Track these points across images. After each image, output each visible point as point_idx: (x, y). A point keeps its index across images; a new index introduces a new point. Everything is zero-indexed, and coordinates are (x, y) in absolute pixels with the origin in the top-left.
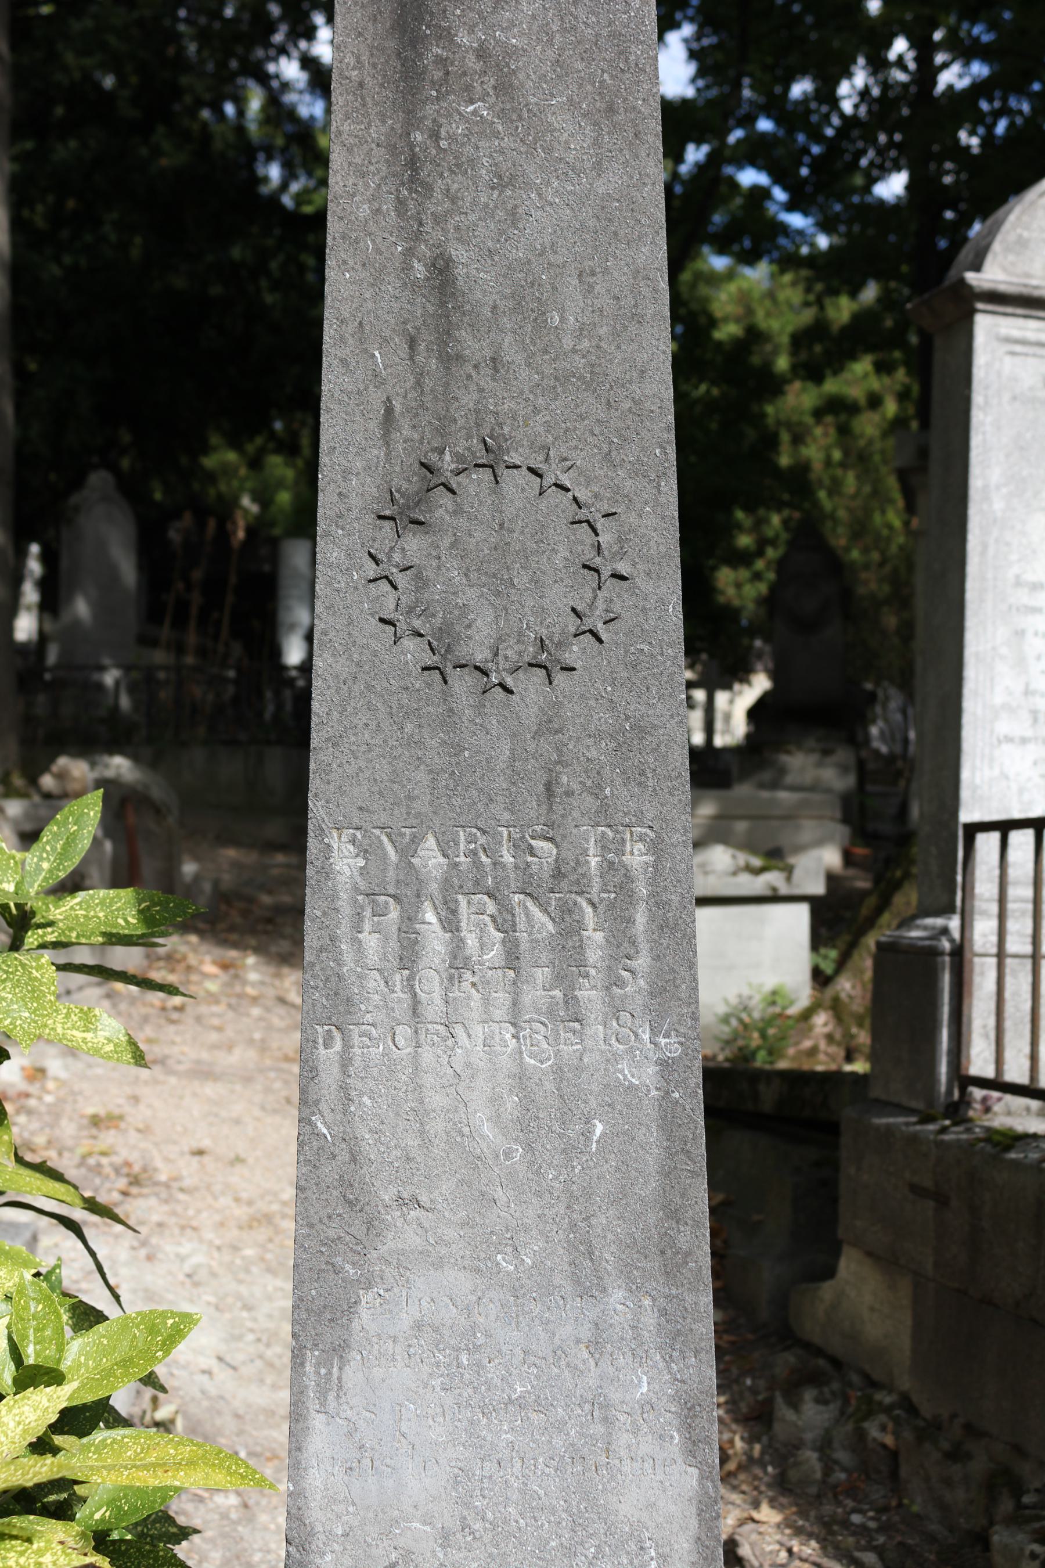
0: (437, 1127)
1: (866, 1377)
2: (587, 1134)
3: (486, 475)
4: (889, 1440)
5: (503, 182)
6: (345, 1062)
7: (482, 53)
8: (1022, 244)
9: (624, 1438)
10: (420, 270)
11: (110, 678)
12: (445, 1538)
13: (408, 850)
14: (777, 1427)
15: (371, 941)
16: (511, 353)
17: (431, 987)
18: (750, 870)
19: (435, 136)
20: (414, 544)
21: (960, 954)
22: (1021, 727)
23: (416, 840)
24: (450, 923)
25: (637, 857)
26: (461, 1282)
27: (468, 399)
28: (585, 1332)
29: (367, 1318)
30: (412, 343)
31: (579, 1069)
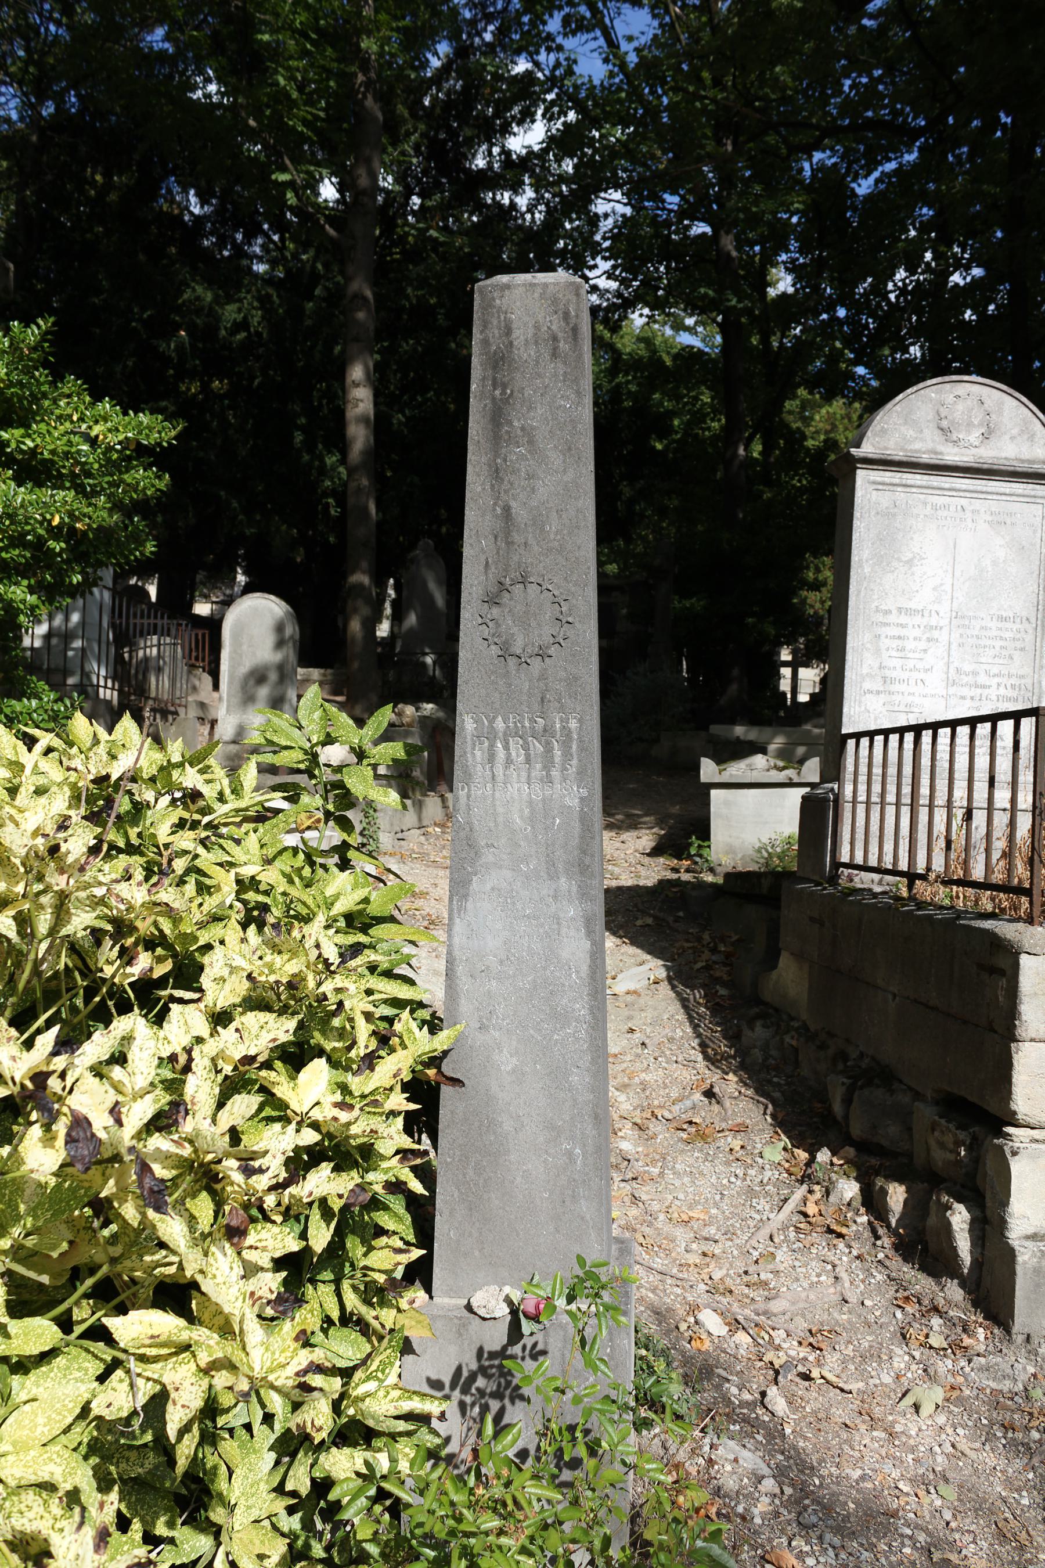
0: (500, 819)
1: (789, 1015)
2: (554, 823)
3: (521, 586)
4: (794, 1043)
5: (530, 477)
6: (469, 796)
7: (523, 429)
8: (884, 431)
9: (564, 930)
10: (499, 511)
11: (429, 660)
12: (501, 962)
13: (492, 721)
14: (743, 1039)
15: (478, 753)
16: (531, 541)
17: (499, 770)
18: (776, 768)
19: (505, 460)
20: (495, 611)
21: (836, 801)
22: (878, 685)
23: (495, 718)
24: (506, 748)
25: (573, 724)
26: (508, 874)
27: (516, 558)
28: (552, 893)
29: (475, 885)
30: (496, 537)
31: (551, 800)
